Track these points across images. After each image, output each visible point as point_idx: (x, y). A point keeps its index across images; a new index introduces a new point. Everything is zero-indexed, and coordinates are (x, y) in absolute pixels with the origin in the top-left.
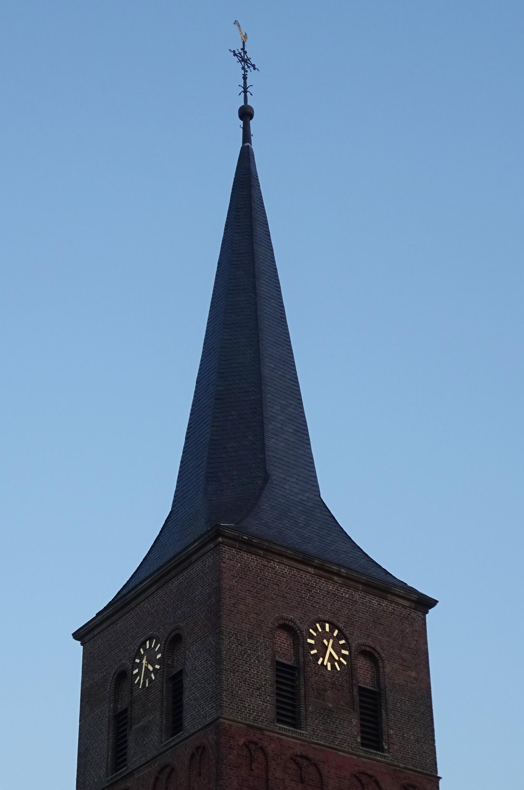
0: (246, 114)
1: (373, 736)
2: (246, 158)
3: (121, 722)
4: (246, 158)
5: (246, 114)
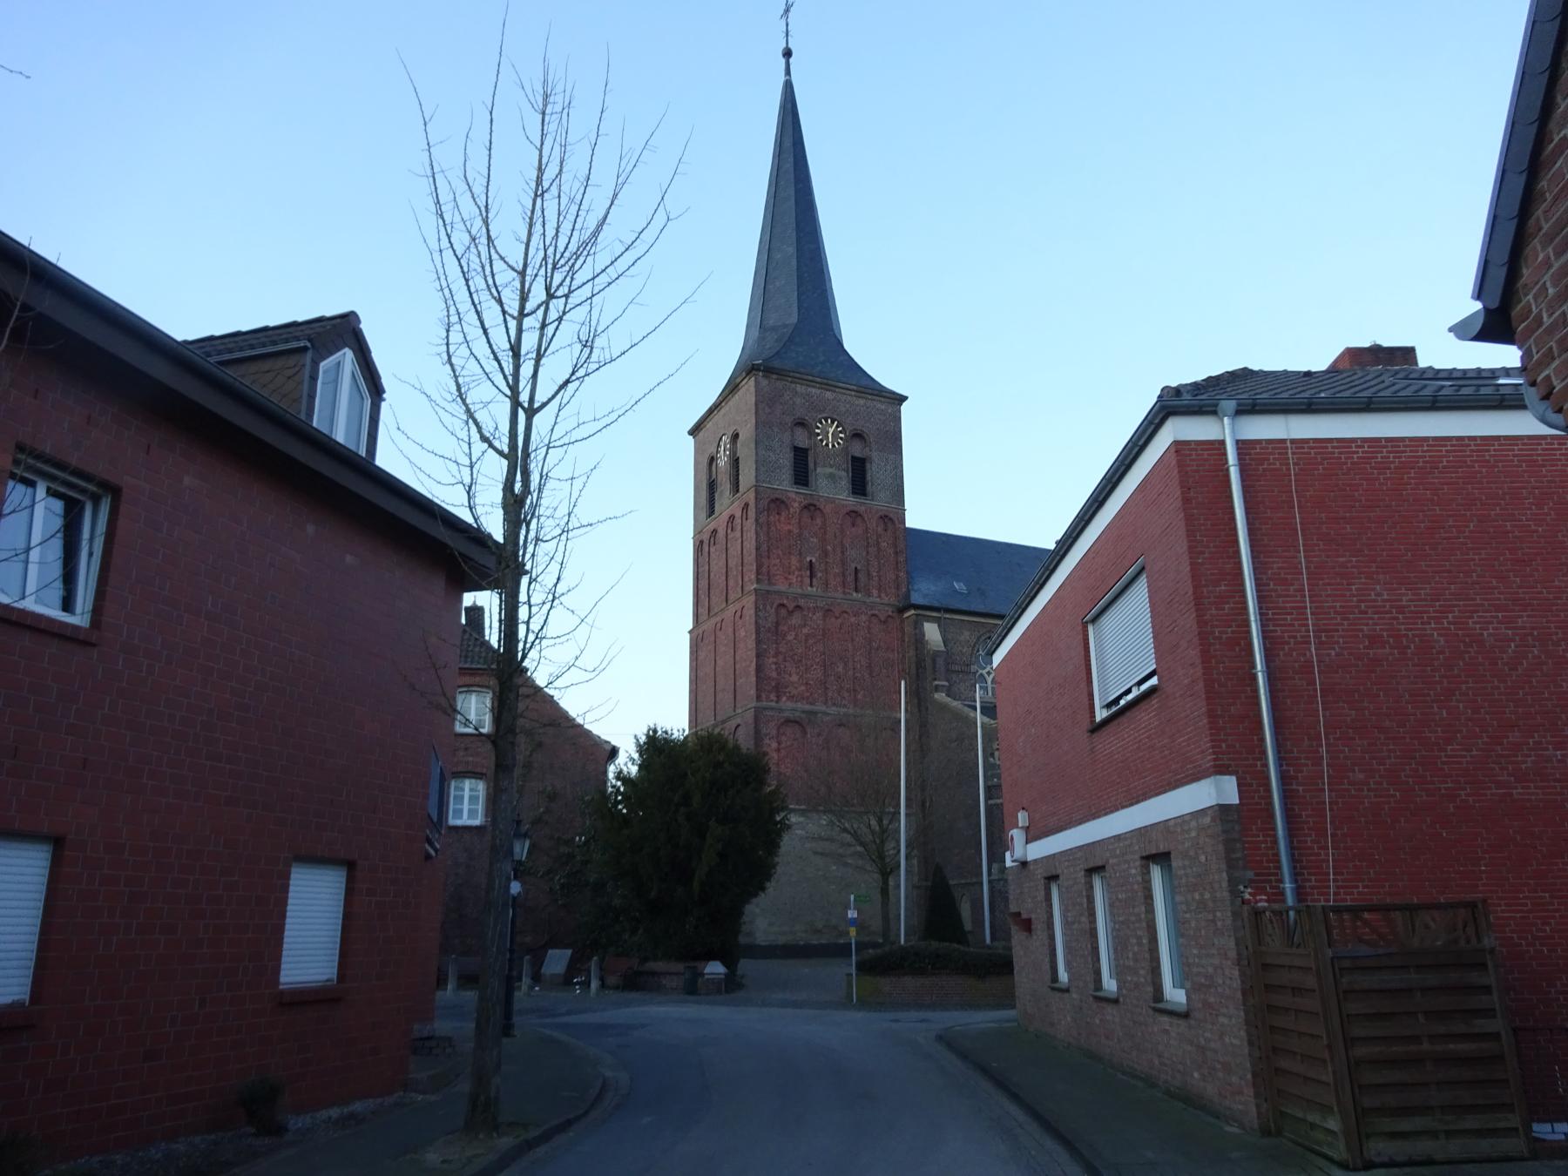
0: (788, 54)
1: (859, 485)
2: (788, 89)
3: (712, 486)
4: (788, 89)
5: (788, 54)
